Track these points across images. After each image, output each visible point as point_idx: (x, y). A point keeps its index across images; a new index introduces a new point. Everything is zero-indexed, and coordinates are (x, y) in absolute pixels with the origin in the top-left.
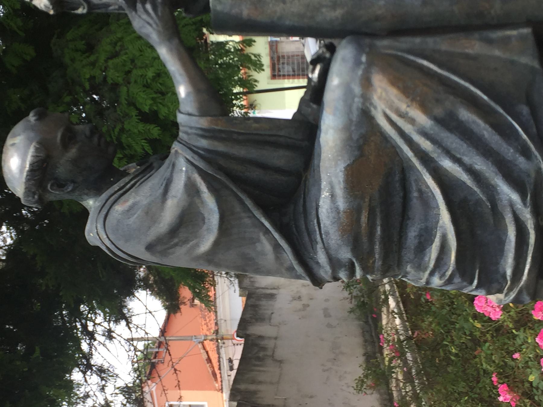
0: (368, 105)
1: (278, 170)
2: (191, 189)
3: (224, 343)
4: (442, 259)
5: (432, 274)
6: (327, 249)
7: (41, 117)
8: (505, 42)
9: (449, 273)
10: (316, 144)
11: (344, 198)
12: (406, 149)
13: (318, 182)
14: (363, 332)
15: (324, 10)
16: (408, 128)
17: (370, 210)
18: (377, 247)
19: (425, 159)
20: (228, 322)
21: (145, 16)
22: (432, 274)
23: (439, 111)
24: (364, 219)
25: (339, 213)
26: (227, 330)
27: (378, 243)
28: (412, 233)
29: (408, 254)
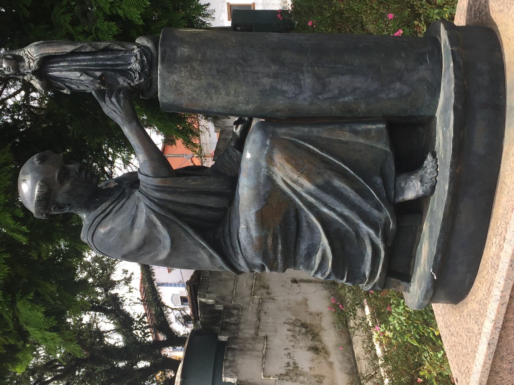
0: (271, 173)
1: (209, 208)
2: (150, 223)
3: (206, 160)
4: (323, 264)
5: (316, 273)
6: (245, 259)
7: (42, 160)
8: (367, 134)
9: (327, 273)
10: (236, 197)
11: (255, 230)
12: (298, 200)
13: (238, 217)
15: (240, 105)
16: (299, 189)
17: (273, 236)
18: (279, 256)
19: (311, 207)
20: (208, 145)
21: (111, 106)
22: (316, 273)
23: (320, 181)
24: (270, 241)
25: (252, 238)
26: (208, 151)
27: (280, 254)
28: (303, 247)
29: (301, 259)
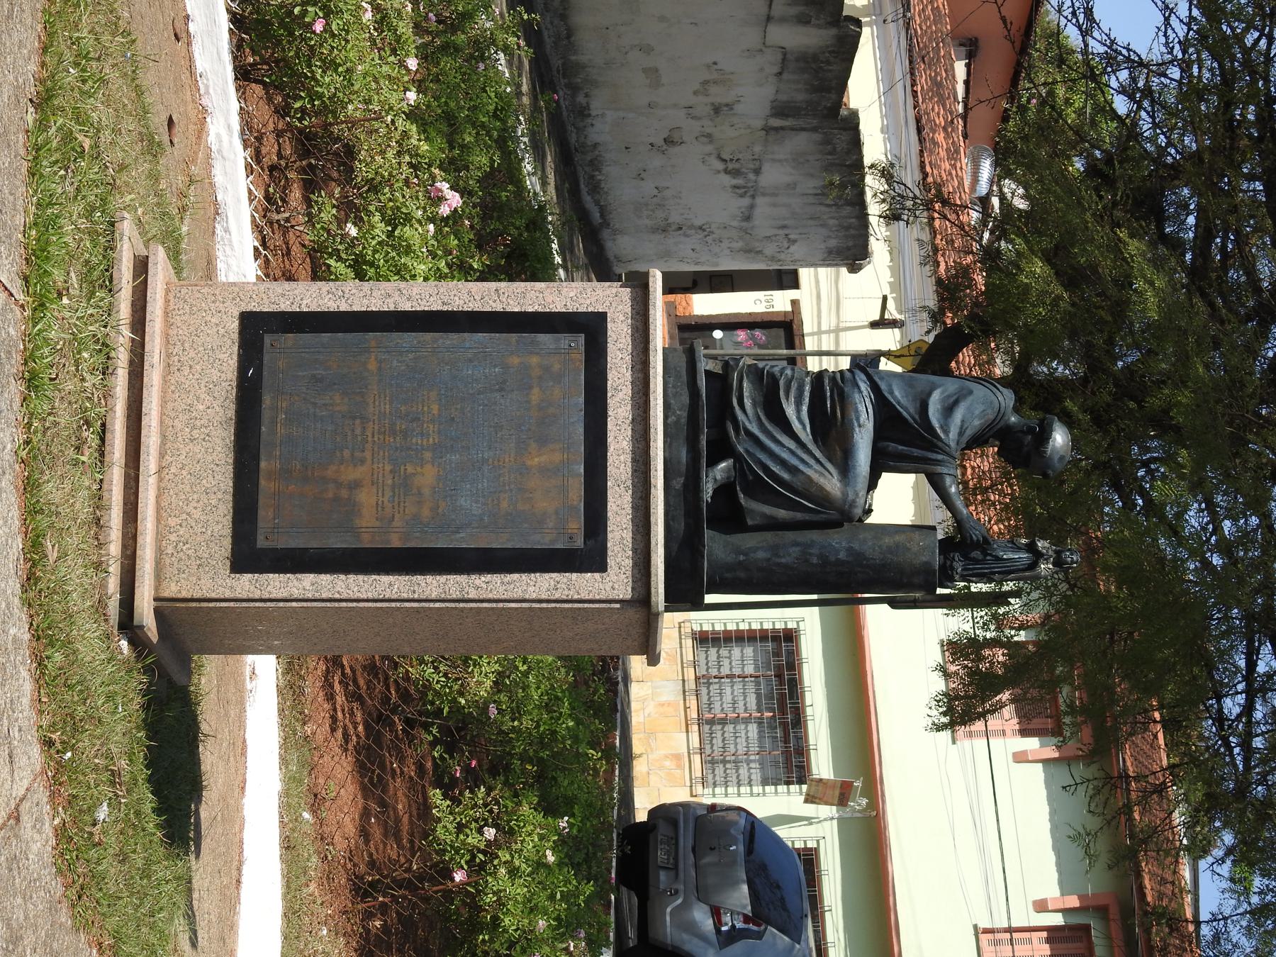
2: (946, 432)
12: (818, 454)
14: (569, 36)
23: (801, 477)
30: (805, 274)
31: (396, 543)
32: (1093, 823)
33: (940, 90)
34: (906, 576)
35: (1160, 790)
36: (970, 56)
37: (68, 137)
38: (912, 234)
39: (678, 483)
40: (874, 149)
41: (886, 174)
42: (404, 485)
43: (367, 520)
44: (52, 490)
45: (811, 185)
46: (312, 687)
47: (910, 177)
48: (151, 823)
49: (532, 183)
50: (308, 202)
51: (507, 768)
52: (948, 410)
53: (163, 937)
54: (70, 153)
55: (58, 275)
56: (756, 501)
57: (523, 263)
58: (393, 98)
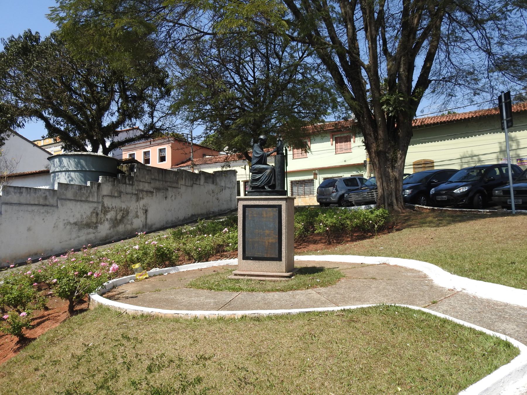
30: (238, 180)
31: (277, 236)
32: (320, 136)
33: (210, 160)
34: (283, 161)
35: (315, 126)
36: (205, 155)
37: (216, 285)
38: (232, 164)
39: (268, 194)
40: (219, 169)
41: (223, 167)
42: (269, 235)
43: (274, 241)
44: (269, 288)
45: (224, 178)
46: (299, 251)
47: (223, 164)
48: (320, 274)
49: (224, 219)
50: (226, 251)
51: (312, 222)
52: (257, 153)
53: (337, 272)
54: (218, 285)
55: (237, 287)
56: (271, 182)
57: (236, 220)
58: (211, 238)
